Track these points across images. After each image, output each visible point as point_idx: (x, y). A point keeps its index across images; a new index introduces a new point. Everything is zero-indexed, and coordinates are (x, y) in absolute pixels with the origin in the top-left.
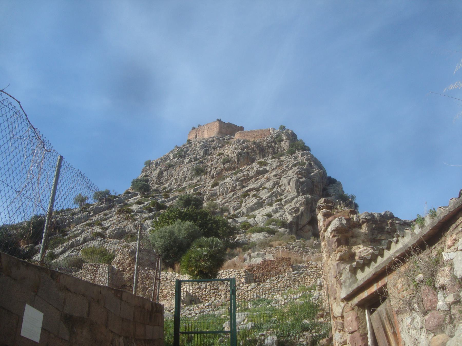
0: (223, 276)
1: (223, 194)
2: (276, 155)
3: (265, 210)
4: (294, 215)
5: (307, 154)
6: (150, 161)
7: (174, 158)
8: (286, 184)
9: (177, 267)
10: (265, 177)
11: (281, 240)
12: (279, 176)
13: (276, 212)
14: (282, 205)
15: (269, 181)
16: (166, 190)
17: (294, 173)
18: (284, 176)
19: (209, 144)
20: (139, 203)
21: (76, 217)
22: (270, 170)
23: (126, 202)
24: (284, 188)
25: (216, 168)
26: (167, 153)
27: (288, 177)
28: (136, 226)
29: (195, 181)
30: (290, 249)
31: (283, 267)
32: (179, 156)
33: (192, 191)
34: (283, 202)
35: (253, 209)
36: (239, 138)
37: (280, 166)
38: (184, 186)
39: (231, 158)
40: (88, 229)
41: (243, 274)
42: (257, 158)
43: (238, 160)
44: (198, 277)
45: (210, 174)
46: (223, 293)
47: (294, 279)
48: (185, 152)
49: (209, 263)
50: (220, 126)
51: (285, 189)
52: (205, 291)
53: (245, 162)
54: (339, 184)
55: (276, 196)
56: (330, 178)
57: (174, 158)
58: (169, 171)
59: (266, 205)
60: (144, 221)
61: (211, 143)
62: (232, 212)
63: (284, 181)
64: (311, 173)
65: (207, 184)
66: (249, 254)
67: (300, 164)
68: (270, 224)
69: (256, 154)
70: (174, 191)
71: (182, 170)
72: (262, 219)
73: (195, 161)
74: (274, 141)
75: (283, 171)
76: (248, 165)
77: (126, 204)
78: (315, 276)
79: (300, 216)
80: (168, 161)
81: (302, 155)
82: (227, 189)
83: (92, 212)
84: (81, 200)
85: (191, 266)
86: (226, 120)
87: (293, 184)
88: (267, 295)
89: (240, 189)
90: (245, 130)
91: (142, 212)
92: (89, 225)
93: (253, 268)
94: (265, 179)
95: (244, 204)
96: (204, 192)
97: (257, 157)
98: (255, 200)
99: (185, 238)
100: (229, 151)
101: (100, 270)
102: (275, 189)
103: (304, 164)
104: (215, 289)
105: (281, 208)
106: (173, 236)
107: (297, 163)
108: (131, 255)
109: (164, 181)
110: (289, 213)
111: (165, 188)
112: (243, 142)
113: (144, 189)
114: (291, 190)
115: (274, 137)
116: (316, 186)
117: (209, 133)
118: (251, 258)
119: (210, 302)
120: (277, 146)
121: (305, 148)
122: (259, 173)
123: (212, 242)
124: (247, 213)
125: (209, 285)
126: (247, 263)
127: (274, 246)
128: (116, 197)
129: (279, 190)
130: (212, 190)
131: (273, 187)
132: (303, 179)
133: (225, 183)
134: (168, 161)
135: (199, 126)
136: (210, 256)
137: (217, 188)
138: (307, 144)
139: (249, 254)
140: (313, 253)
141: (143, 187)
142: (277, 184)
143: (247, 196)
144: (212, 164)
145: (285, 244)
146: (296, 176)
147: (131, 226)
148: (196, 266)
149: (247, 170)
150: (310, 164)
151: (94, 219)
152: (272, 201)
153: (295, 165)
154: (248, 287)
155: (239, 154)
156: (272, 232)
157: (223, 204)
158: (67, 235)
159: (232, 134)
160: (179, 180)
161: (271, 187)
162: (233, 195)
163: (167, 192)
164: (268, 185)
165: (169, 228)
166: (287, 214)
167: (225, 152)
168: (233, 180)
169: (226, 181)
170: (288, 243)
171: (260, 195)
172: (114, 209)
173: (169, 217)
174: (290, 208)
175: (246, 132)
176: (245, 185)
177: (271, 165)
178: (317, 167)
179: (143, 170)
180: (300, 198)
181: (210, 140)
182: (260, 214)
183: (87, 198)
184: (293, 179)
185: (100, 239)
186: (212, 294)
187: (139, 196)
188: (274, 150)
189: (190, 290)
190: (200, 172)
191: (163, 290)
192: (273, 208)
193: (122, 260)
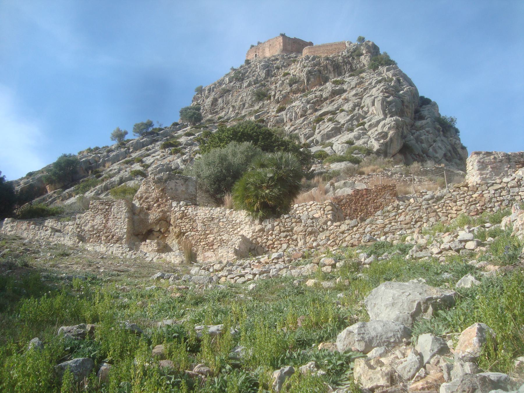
0: (298, 212)
1: (291, 120)
2: (354, 72)
3: (345, 137)
4: (382, 141)
5: (394, 69)
6: (202, 87)
7: (230, 82)
10: (343, 97)
12: (360, 96)
13: (358, 138)
14: (366, 129)
15: (347, 102)
16: (222, 120)
17: (379, 91)
18: (367, 96)
19: (272, 64)
20: (188, 134)
21: (112, 154)
22: (348, 89)
24: (367, 109)
25: (281, 91)
27: (371, 96)
28: (184, 161)
29: (256, 107)
30: (388, 176)
31: (385, 198)
32: (236, 79)
33: (253, 118)
34: (366, 126)
35: (329, 136)
36: (308, 54)
37: (360, 83)
39: (300, 78)
40: (127, 168)
41: (329, 208)
42: (331, 77)
43: (308, 80)
44: (261, 212)
45: (274, 98)
46: (299, 237)
47: (427, 209)
48: (243, 74)
49: (276, 190)
52: (272, 235)
54: (435, 105)
55: (358, 120)
56: (422, 98)
57: (230, 82)
58: (224, 98)
60: (194, 155)
61: (274, 62)
62: (303, 141)
63: (367, 101)
64: (399, 91)
66: (332, 184)
67: (385, 81)
68: (352, 153)
69: (330, 72)
70: (232, 121)
71: (240, 95)
72: (342, 147)
73: (255, 84)
74: (351, 56)
75: (365, 90)
77: (173, 137)
78: (466, 202)
79: (389, 143)
80: (224, 86)
81: (388, 70)
82: (296, 114)
85: (248, 197)
86: (291, 35)
88: (390, 236)
89: (311, 114)
91: (191, 144)
92: (127, 163)
93: (342, 200)
94: (343, 99)
95: (317, 131)
96: (267, 119)
97: (331, 76)
98: (331, 125)
99: (243, 164)
101: (114, 209)
102: (356, 111)
103: (391, 80)
104: (288, 231)
107: (382, 79)
108: (159, 184)
109: (219, 109)
111: (220, 118)
112: (314, 59)
114: (375, 112)
116: (407, 107)
118: (335, 189)
119: (280, 252)
120: (355, 61)
121: (389, 62)
122: (335, 93)
123: (281, 158)
124: (322, 141)
125: (278, 225)
126: (331, 194)
127: (366, 172)
128: (160, 129)
129: (360, 112)
130: (278, 116)
131: (353, 109)
132: (391, 98)
133: (293, 107)
134: (224, 86)
135: (259, 43)
137: (283, 113)
139: (332, 184)
140: (420, 181)
141: (193, 116)
142: (358, 105)
143: (320, 121)
144: (276, 87)
145: (381, 169)
146: (381, 94)
147: (179, 161)
148: (257, 196)
149: (320, 90)
150: (398, 80)
151: (134, 155)
152: (352, 125)
153: (379, 82)
154: (340, 226)
155: (309, 72)
157: (291, 132)
158: (100, 176)
159: (299, 51)
160: (237, 108)
161: (350, 109)
162: (304, 121)
163: (223, 122)
166: (373, 140)
167: (292, 72)
168: (302, 103)
169: (294, 104)
170: (384, 169)
171: (337, 119)
173: (219, 139)
174: (376, 133)
175: (316, 47)
176: (318, 108)
177: (349, 83)
178: (408, 84)
179: (194, 98)
180: (388, 120)
181: (273, 58)
182: (339, 142)
185: (140, 178)
186: (282, 239)
187: (189, 127)
188: (351, 67)
189: (248, 233)
190: (261, 96)
191: (208, 234)
192: (355, 133)
193: (146, 192)
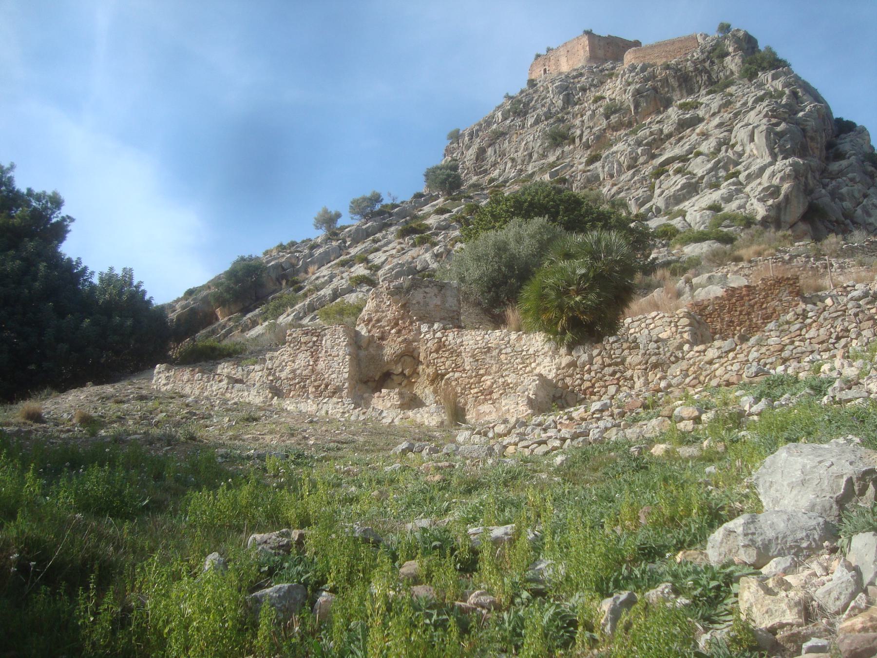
0: (632, 331)
1: (612, 176)
2: (715, 85)
3: (706, 198)
4: (770, 202)
5: (785, 74)
6: (458, 131)
7: (505, 119)
8: (746, 140)
10: (698, 131)
11: (760, 244)
12: (727, 127)
13: (728, 199)
14: (741, 184)
15: (707, 139)
16: (495, 183)
17: (761, 115)
18: (739, 125)
20: (441, 211)
21: (318, 252)
22: (707, 116)
24: (741, 149)
25: (591, 128)
26: (489, 112)
28: (437, 256)
29: (552, 159)
30: (784, 262)
31: (781, 301)
32: (515, 113)
33: (547, 177)
34: (742, 177)
35: (678, 198)
37: (727, 105)
38: (530, 172)
39: (622, 103)
41: (685, 321)
42: (675, 98)
43: (637, 106)
45: (581, 140)
46: (637, 373)
47: (856, 315)
48: (526, 105)
49: (592, 296)
52: (589, 371)
54: (863, 131)
55: (726, 167)
56: (839, 121)
57: (505, 119)
58: (497, 146)
60: (453, 246)
61: (576, 80)
62: (634, 210)
63: (740, 134)
64: (796, 113)
65: (578, 160)
66: (688, 281)
67: (771, 96)
68: (719, 225)
69: (673, 90)
70: (512, 184)
71: (522, 139)
72: (701, 216)
73: (547, 119)
74: (708, 58)
75: (736, 115)
76: (659, 112)
77: (415, 217)
80: (494, 126)
81: (774, 78)
82: (620, 164)
83: (348, 239)
84: (328, 220)
85: (546, 310)
86: (602, 31)
87: (760, 139)
90: (643, 45)
91: (447, 228)
92: (343, 264)
93: (706, 307)
94: (698, 135)
95: (657, 192)
96: (571, 176)
97: (676, 95)
98: (681, 180)
99: (534, 256)
100: (616, 90)
101: (327, 342)
102: (722, 154)
103: (781, 94)
104: (617, 364)
105: (738, 191)
107: (765, 94)
109: (489, 166)
110: (759, 200)
111: (492, 180)
112: (643, 69)
113: (450, 183)
114: (756, 152)
115: (708, 48)
117: (570, 63)
118: (693, 288)
119: (605, 399)
120: (715, 67)
121: (775, 64)
122: (684, 125)
123: (599, 241)
124: (667, 207)
125: (599, 354)
127: (745, 257)
128: (394, 206)
129: (730, 153)
130: (589, 171)
132: (783, 126)
133: (613, 153)
134: (494, 126)
135: (549, 50)
136: (594, 277)
137: (598, 164)
139: (688, 281)
140: (841, 267)
141: (447, 181)
142: (725, 143)
143: (662, 174)
145: (772, 251)
146: (765, 121)
147: (428, 256)
148: (560, 308)
149: (658, 122)
150: (794, 94)
151: (353, 251)
152: (718, 178)
153: (760, 99)
154: (704, 351)
155: (638, 93)
156: (728, 239)
157: (613, 196)
158: (301, 288)
159: (618, 58)
160: (519, 161)
161: (712, 150)
162: (634, 175)
163: (497, 186)
165: (491, 237)
166: (754, 201)
167: (607, 94)
168: (629, 145)
169: (615, 149)
172: (392, 229)
173: (493, 216)
174: (760, 188)
175: (647, 48)
176: (657, 152)
177: (707, 105)
180: (780, 164)
181: (575, 73)
182: (696, 208)
184: (760, 129)
186: (607, 378)
187: (441, 200)
189: (550, 371)
190: (559, 139)
191: (483, 375)
192: (723, 190)
193: (377, 311)
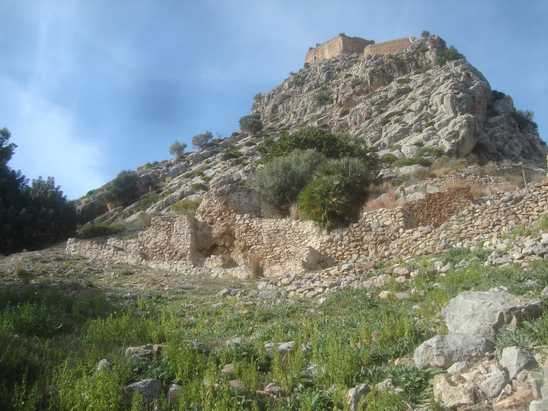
0: (367, 220)
1: (356, 124)
2: (420, 69)
3: (414, 138)
4: (453, 141)
5: (463, 63)
6: (260, 94)
8: (439, 102)
9: (293, 210)
10: (409, 96)
12: (427, 94)
13: (428, 139)
14: (435, 129)
15: (414, 102)
16: (283, 127)
17: (448, 88)
18: (434, 93)
19: (333, 66)
20: (249, 144)
21: (171, 169)
22: (415, 88)
23: (233, 144)
24: (435, 108)
25: (343, 94)
26: (280, 83)
27: (439, 93)
28: (246, 172)
29: (319, 112)
31: (459, 202)
32: (296, 83)
33: (315, 124)
34: (436, 126)
36: (370, 53)
37: (427, 81)
39: (362, 79)
41: (401, 214)
42: (395, 76)
43: (372, 81)
46: (370, 246)
47: (505, 211)
48: (303, 79)
49: (344, 198)
50: (344, 42)
51: (437, 109)
52: (341, 245)
53: (381, 83)
54: (509, 98)
55: (426, 119)
56: (495, 92)
58: (285, 104)
59: (414, 131)
60: (256, 166)
61: (334, 64)
62: (369, 145)
63: (435, 99)
64: (469, 87)
66: (402, 189)
67: (454, 76)
68: (422, 155)
69: (394, 71)
70: (294, 127)
71: (301, 100)
72: (411, 149)
73: (316, 88)
74: (416, 52)
75: (433, 87)
76: (385, 85)
77: (233, 148)
79: (461, 143)
80: (283, 92)
81: (456, 65)
82: (361, 116)
83: (191, 161)
85: (314, 207)
86: (351, 34)
87: (447, 102)
88: (467, 241)
89: (377, 116)
91: (253, 154)
93: (413, 206)
94: (409, 99)
95: (384, 134)
96: (331, 124)
97: (396, 75)
98: (399, 127)
100: (359, 71)
101: (177, 225)
102: (424, 111)
103: (460, 75)
104: (358, 241)
105: (434, 134)
106: (289, 171)
107: (450, 75)
108: (221, 197)
109: (280, 116)
110: (446, 140)
111: (281, 125)
112: (376, 58)
113: (255, 127)
114: (445, 110)
116: (479, 103)
117: (331, 53)
118: (405, 194)
120: (420, 58)
122: (400, 93)
123: (347, 164)
124: (390, 144)
125: (347, 235)
126: (401, 200)
127: (438, 175)
128: (220, 140)
129: (429, 111)
130: (342, 120)
132: (461, 95)
133: (357, 109)
134: (283, 92)
135: (318, 45)
137: (347, 116)
138: (459, 52)
139: (402, 189)
141: (253, 125)
142: (425, 104)
143: (387, 123)
145: (454, 171)
146: (450, 91)
147: (241, 172)
148: (323, 205)
149: (385, 91)
150: (468, 75)
151: (194, 168)
152: (421, 126)
153: (447, 78)
154: (412, 233)
155: (372, 73)
157: (356, 136)
158: (161, 191)
160: (298, 114)
161: (418, 108)
162: (369, 123)
163: (284, 129)
164: (414, 106)
166: (444, 140)
167: (354, 73)
168: (367, 105)
169: (358, 107)
171: (404, 120)
174: (447, 132)
175: (378, 45)
176: (384, 109)
177: (415, 81)
178: (478, 78)
179: (253, 106)
180: (459, 118)
181: (334, 60)
182: (407, 144)
183: (185, 146)
184: (447, 96)
187: (249, 137)
188: (417, 64)
189: (316, 245)
190: (323, 100)
191: (274, 247)
192: (424, 134)
